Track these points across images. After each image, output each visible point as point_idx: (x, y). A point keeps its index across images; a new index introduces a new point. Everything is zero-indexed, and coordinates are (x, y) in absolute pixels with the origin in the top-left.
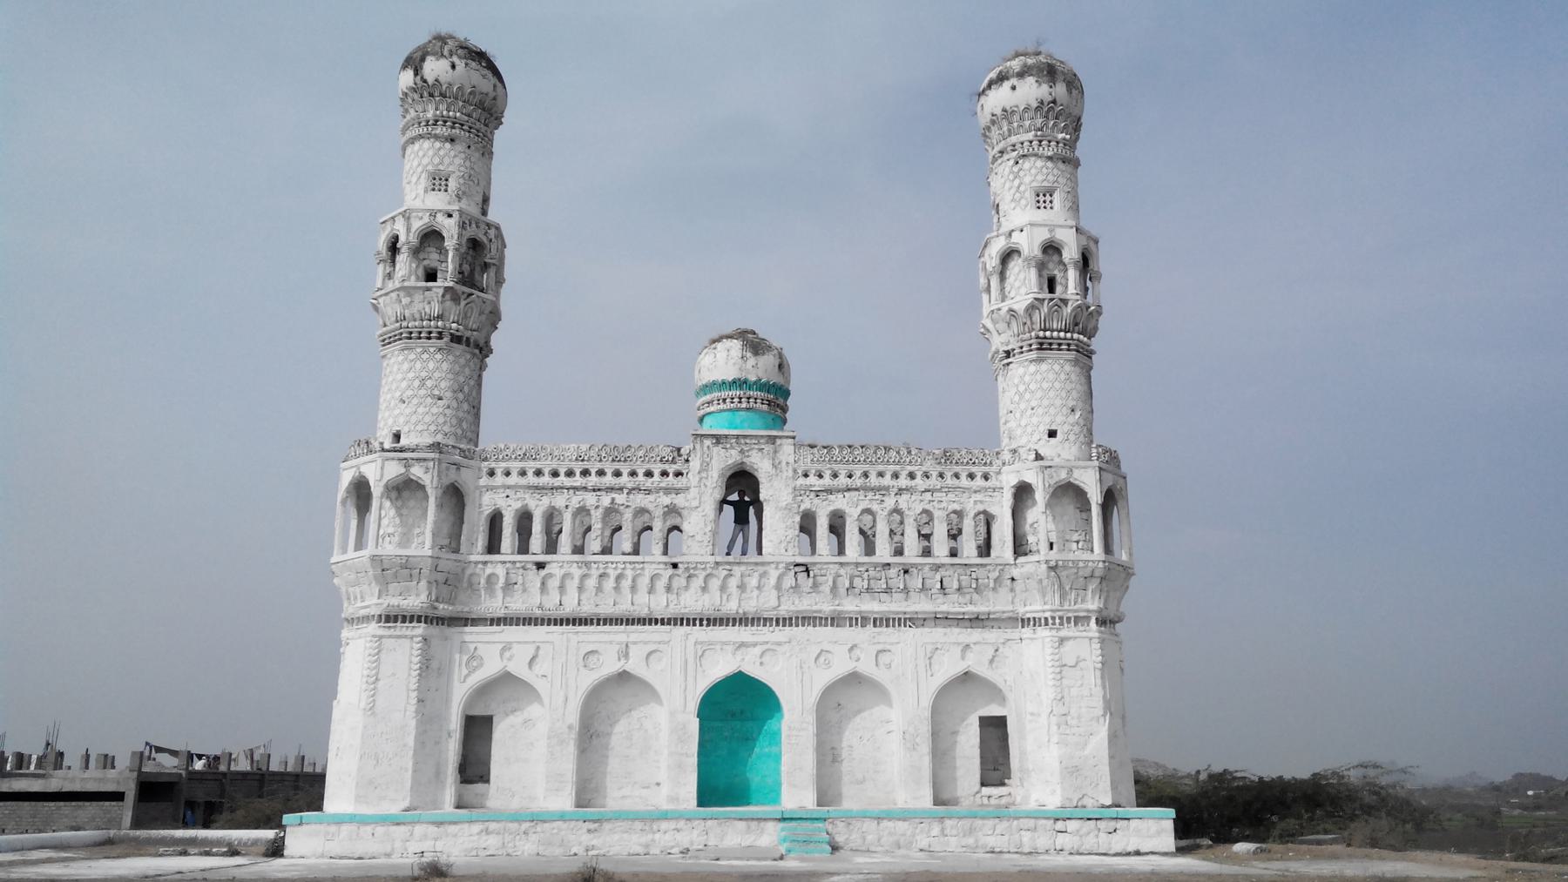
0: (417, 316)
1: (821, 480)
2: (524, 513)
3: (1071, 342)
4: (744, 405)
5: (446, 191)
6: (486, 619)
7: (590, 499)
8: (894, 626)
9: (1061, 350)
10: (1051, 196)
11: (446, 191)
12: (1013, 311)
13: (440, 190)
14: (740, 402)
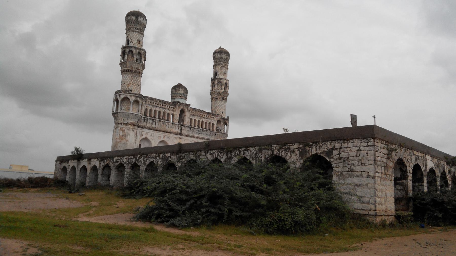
0: (135, 68)
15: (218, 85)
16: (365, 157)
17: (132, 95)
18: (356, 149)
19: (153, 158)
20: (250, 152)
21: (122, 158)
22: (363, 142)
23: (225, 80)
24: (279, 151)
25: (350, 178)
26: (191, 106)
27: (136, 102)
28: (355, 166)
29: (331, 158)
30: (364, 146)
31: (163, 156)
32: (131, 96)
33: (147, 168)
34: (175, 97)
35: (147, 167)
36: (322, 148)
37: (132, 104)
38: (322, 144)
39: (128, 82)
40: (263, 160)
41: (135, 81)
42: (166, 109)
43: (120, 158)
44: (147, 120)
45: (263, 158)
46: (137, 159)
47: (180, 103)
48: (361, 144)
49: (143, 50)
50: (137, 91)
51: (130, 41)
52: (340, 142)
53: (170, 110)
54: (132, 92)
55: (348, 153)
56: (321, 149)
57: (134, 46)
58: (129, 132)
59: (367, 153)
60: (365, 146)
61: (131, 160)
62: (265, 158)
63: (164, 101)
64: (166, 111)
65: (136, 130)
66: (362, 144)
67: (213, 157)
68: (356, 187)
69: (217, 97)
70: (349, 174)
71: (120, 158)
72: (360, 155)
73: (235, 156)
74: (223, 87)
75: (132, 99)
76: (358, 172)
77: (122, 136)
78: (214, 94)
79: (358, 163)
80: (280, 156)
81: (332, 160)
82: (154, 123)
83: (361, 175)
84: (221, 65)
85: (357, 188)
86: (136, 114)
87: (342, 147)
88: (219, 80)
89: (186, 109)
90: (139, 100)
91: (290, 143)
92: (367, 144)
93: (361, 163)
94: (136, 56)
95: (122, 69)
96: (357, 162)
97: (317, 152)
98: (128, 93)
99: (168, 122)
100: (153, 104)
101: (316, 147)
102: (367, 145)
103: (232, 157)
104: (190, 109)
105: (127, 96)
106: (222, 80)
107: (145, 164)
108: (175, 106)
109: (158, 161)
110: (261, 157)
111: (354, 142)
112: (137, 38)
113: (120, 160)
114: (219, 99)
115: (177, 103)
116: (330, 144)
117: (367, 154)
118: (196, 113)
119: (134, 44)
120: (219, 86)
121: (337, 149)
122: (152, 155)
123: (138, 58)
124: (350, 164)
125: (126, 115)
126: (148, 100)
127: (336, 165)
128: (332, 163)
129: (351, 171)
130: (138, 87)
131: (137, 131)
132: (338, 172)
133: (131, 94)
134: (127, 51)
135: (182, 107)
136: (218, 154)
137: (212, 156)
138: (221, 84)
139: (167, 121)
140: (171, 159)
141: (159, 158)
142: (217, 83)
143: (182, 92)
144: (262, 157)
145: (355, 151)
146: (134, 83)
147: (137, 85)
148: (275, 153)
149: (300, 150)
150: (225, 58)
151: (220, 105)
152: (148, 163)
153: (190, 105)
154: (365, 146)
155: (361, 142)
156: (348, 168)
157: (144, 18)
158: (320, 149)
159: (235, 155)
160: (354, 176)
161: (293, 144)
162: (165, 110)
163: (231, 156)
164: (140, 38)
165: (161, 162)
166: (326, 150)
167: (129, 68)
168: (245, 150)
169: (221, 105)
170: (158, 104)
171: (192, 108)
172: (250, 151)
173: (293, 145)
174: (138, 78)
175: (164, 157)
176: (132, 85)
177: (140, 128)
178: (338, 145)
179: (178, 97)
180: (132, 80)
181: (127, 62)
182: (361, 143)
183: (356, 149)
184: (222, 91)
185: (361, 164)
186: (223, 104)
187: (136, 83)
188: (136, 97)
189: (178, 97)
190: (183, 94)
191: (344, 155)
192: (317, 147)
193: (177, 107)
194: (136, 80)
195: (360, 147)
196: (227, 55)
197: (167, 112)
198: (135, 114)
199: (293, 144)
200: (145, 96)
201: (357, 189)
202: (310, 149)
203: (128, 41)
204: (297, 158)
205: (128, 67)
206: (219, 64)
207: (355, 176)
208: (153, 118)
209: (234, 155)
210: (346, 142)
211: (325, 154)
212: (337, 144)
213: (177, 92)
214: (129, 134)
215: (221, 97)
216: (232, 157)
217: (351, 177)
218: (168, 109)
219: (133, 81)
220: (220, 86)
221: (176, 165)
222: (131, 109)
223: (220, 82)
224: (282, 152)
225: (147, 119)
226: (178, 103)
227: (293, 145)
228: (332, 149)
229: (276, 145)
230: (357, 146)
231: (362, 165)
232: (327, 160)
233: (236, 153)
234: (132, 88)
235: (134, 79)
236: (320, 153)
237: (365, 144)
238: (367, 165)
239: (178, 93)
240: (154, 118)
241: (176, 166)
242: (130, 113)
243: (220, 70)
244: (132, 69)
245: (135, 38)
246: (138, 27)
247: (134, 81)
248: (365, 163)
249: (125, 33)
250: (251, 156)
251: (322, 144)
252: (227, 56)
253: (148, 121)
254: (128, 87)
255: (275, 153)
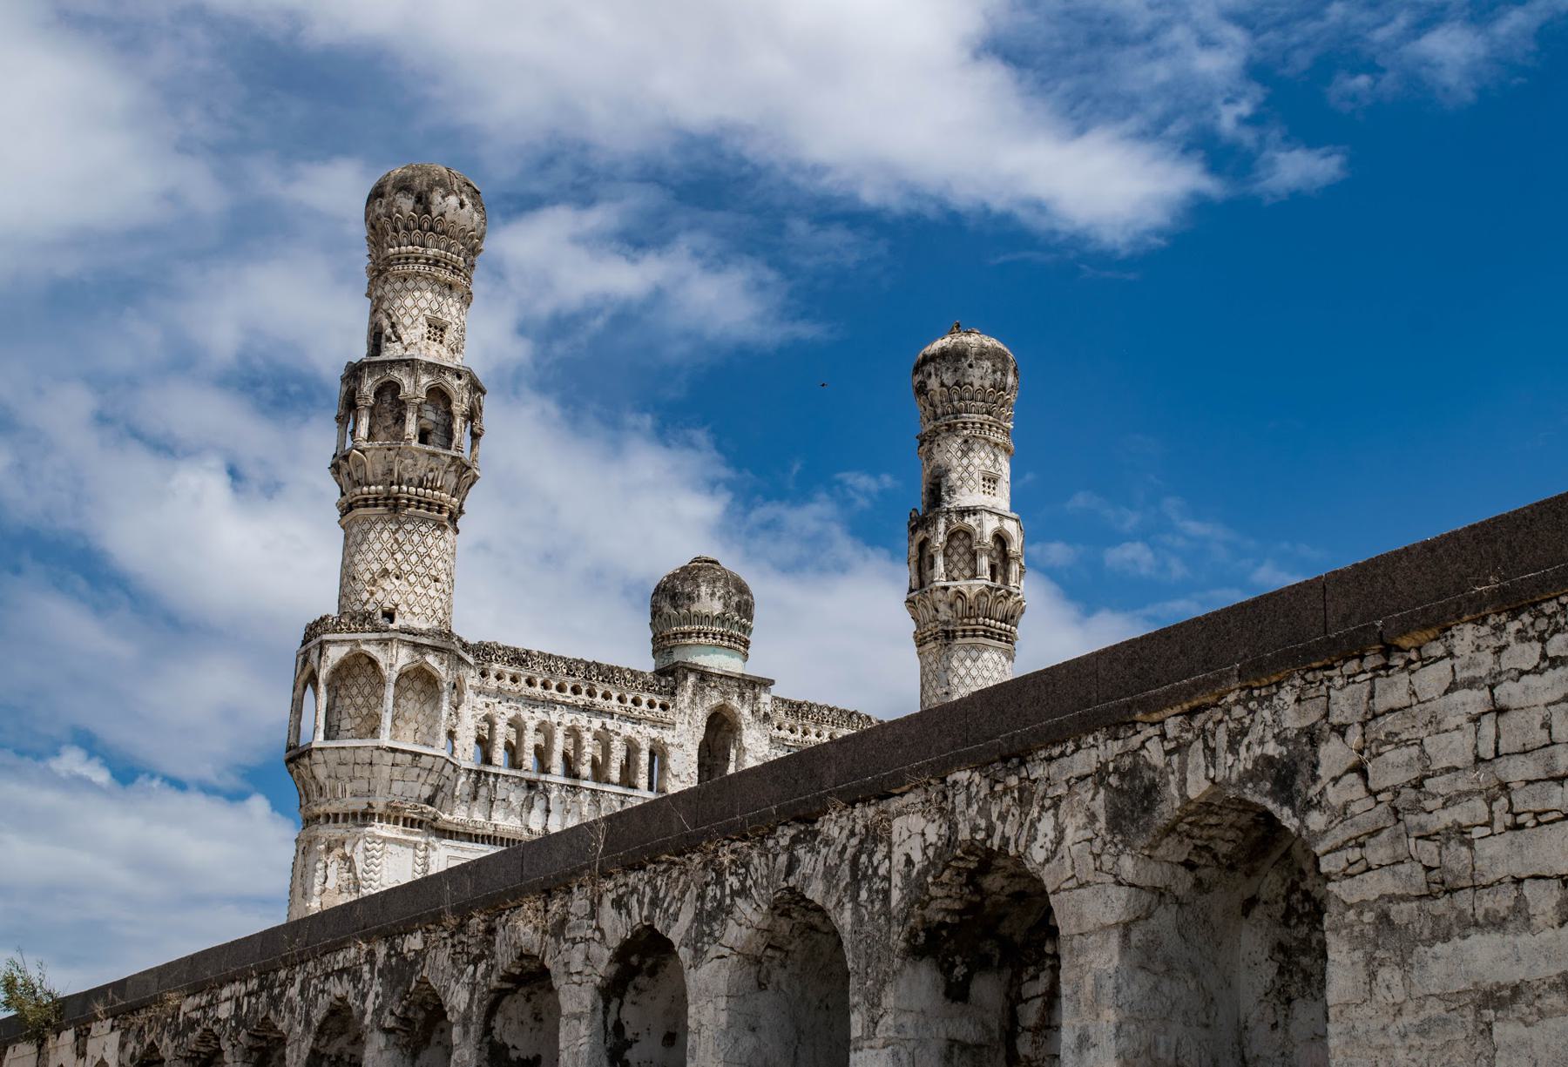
0: (416, 481)
1: (532, 688)
2: (637, 748)
3: (422, 499)
4: (726, 643)
5: (441, 342)
6: (318, 817)
7: (583, 720)
8: (489, 843)
9: (977, 636)
10: (994, 482)
11: (441, 342)
12: (961, 593)
13: (435, 340)
14: (714, 639)
15: (950, 551)
16: (1536, 754)
17: (391, 640)
18: (1475, 699)
19: (345, 976)
20: (824, 851)
21: (212, 998)
22: (1511, 639)
23: (996, 518)
24: (984, 812)
25: (1439, 947)
26: (775, 690)
27: (422, 682)
28: (1470, 844)
29: (1309, 805)
30: (1522, 673)
31: (388, 956)
32: (384, 643)
33: (322, 1051)
34: (673, 642)
35: (317, 1040)
36: (1246, 741)
37: (390, 692)
38: (1251, 712)
39: (375, 567)
40: (896, 895)
41: (414, 558)
42: (612, 715)
43: (204, 1000)
44: (495, 786)
45: (896, 879)
46: (277, 991)
47: (704, 676)
48: (1498, 662)
49: (459, 377)
50: (429, 612)
51: (389, 331)
52: (1364, 672)
53: (638, 721)
54: (398, 622)
55: (1415, 750)
56: (1242, 750)
57: (407, 355)
58: (377, 862)
59: (1547, 725)
60: (1527, 672)
61: (249, 1003)
62: (906, 877)
63: (598, 666)
64: (611, 724)
65: (422, 854)
66: (1506, 662)
67: (630, 917)
68: (1489, 1014)
69: (950, 628)
70: (1436, 919)
71: (204, 1000)
72: (1502, 750)
73: (743, 892)
74: (984, 562)
75: (394, 660)
76: (1492, 885)
77: (341, 892)
78: (932, 612)
79: (1491, 812)
80: (996, 848)
81: (1316, 820)
82: (539, 804)
83: (1520, 908)
84: (965, 432)
85: (1497, 1019)
86: (419, 755)
87: (1380, 705)
88: (956, 523)
89: (746, 711)
90: (436, 665)
91: (1054, 744)
92: (1537, 646)
93: (1510, 811)
94: (419, 410)
95: (343, 494)
96: (1479, 807)
97: (1220, 774)
98: (367, 626)
99: (629, 792)
100: (529, 691)
101: (1212, 744)
102: (1544, 656)
103: (728, 901)
104: (768, 709)
105: (364, 647)
106: (970, 521)
107: (308, 1023)
108: (673, 694)
109: (365, 990)
110: (888, 878)
111: (1451, 655)
112: (428, 312)
113: (205, 1012)
114: (964, 636)
115: (686, 678)
116: (1298, 700)
117: (1545, 733)
118: (814, 731)
119: (409, 344)
120: (956, 558)
121: (1341, 730)
122: (340, 957)
123: (430, 427)
124: (1437, 833)
125: (356, 763)
126: (496, 666)
127: (1343, 854)
128: (1319, 849)
129: (1441, 886)
130: (432, 592)
131: (426, 857)
132: (1361, 906)
133: (385, 635)
134: (368, 386)
135: (714, 699)
136: (655, 889)
137: (624, 912)
138: (971, 546)
139: (620, 790)
140: (427, 968)
141: (372, 971)
142: (941, 538)
143: (716, 607)
144: (889, 872)
145: (1462, 720)
146: (406, 567)
147: (426, 580)
148: (964, 834)
149: (1114, 780)
150: (987, 384)
151: (968, 674)
152: (318, 1015)
153: (772, 682)
154: (1527, 672)
155: (1502, 643)
156: (1428, 869)
157: (464, 197)
158: (1235, 752)
159: (742, 883)
160: (1469, 924)
161: (1071, 746)
162: (608, 721)
163: (723, 896)
164: (440, 310)
165: (380, 997)
166: (1272, 749)
167: (376, 484)
168: (795, 840)
169: (974, 672)
170: (606, 696)
171: (784, 701)
172: (827, 843)
173: (1069, 751)
174: (430, 541)
175: (394, 960)
176: (397, 582)
177: (451, 838)
178: (1346, 702)
179: (690, 642)
180: (393, 554)
181: (369, 449)
182: (1499, 651)
183: (1475, 699)
184: (976, 590)
185: (1509, 819)
186: (991, 665)
187: (420, 569)
188: (416, 646)
189: (690, 642)
190: (722, 619)
191: (1392, 768)
192: (1213, 735)
193: (685, 696)
194: (422, 550)
195: (1492, 688)
196: (999, 366)
197: (618, 734)
198: (411, 753)
199: (1071, 746)
200: (481, 643)
201: (1497, 1028)
202: (1175, 758)
203: (377, 340)
204: (1098, 843)
205: (371, 479)
206: (951, 428)
207: (1476, 924)
208: (527, 775)
209: (736, 885)
210: (1401, 663)
211: (1268, 786)
212: (1343, 687)
213: (683, 611)
214: (376, 877)
215: (973, 621)
216: (728, 901)
217: (1446, 938)
218: (627, 718)
219: (399, 556)
220: (967, 557)
221: (447, 1009)
222: (387, 721)
223: (961, 537)
224: (1003, 817)
225: (491, 779)
226: (692, 679)
227: (1069, 751)
228: (1312, 736)
229: (968, 773)
230: (1471, 684)
231: (1521, 827)
232: (1286, 823)
233: (748, 870)
234: (396, 598)
235: (407, 547)
236: (1234, 776)
237: (1528, 654)
238: (1554, 815)
239: (688, 619)
240: (534, 776)
241: (445, 1014)
242: (378, 748)
243: (961, 458)
244: (395, 488)
245: (415, 312)
246: (431, 252)
247: (407, 554)
248: (1539, 809)
249: (365, 290)
250: (830, 874)
251: (1246, 707)
252: (994, 372)
253: (501, 794)
254: (372, 594)
255: (964, 834)
